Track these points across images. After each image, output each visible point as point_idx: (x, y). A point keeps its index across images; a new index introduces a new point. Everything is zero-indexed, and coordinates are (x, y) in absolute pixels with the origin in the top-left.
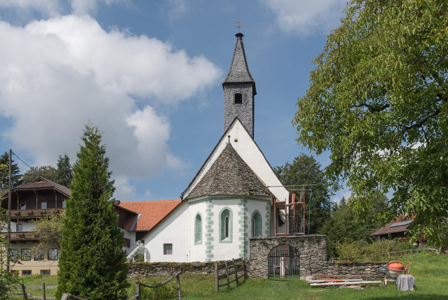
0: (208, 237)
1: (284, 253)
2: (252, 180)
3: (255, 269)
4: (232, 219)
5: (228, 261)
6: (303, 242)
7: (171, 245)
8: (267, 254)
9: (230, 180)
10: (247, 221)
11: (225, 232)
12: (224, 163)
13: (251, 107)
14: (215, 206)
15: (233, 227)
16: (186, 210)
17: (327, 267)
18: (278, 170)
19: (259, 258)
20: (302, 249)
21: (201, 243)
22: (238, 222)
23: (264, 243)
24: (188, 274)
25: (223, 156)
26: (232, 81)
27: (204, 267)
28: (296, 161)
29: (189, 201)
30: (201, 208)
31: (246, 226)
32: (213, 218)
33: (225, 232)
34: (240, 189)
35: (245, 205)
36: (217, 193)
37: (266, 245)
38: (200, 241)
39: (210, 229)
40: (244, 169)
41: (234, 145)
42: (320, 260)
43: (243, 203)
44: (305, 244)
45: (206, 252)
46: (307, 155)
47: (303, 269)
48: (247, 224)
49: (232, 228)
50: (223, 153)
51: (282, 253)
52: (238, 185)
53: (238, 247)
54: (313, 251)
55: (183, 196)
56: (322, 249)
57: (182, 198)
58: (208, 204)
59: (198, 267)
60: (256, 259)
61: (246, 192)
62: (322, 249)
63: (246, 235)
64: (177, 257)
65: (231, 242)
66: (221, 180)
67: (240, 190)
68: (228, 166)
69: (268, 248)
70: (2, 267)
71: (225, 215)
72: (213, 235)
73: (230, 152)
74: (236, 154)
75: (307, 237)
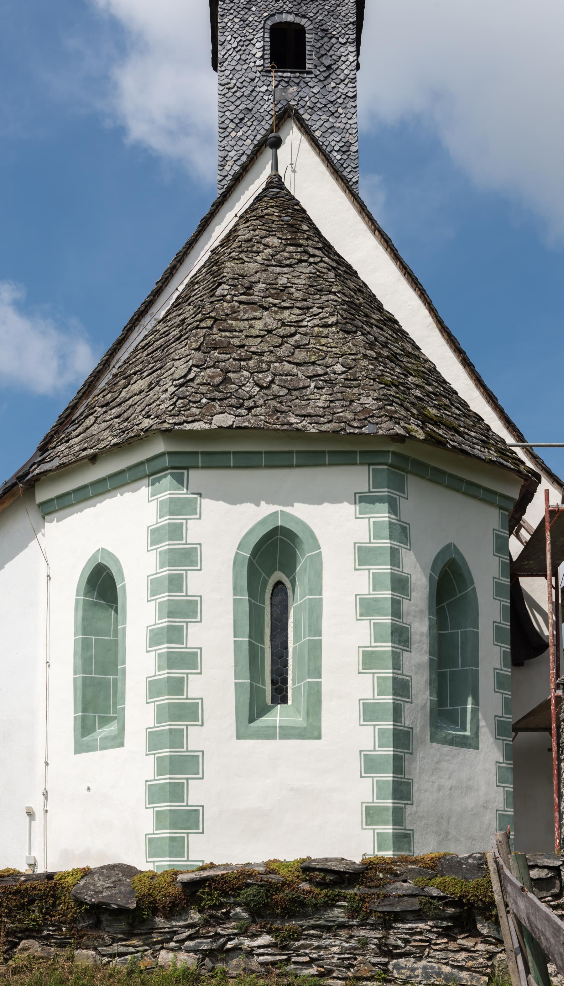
0: (165, 700)
4: (316, 587)
9: (300, 356)
10: (406, 605)
11: (272, 678)
14: (207, 505)
15: (326, 639)
16: (23, 546)
21: (118, 741)
22: (351, 608)
24: (39, 969)
27: (174, 910)
29: (44, 494)
30: (121, 524)
31: (400, 636)
32: (195, 583)
33: (272, 678)
34: (369, 402)
35: (394, 509)
36: (224, 420)
38: (112, 728)
39: (176, 647)
43: (384, 492)
45: (154, 794)
48: (407, 620)
49: (315, 649)
52: (351, 381)
58: (165, 496)
59: (122, 911)
65: (312, 731)
66: (243, 353)
67: (365, 410)
68: (282, 280)
71: (274, 561)
72: (196, 687)
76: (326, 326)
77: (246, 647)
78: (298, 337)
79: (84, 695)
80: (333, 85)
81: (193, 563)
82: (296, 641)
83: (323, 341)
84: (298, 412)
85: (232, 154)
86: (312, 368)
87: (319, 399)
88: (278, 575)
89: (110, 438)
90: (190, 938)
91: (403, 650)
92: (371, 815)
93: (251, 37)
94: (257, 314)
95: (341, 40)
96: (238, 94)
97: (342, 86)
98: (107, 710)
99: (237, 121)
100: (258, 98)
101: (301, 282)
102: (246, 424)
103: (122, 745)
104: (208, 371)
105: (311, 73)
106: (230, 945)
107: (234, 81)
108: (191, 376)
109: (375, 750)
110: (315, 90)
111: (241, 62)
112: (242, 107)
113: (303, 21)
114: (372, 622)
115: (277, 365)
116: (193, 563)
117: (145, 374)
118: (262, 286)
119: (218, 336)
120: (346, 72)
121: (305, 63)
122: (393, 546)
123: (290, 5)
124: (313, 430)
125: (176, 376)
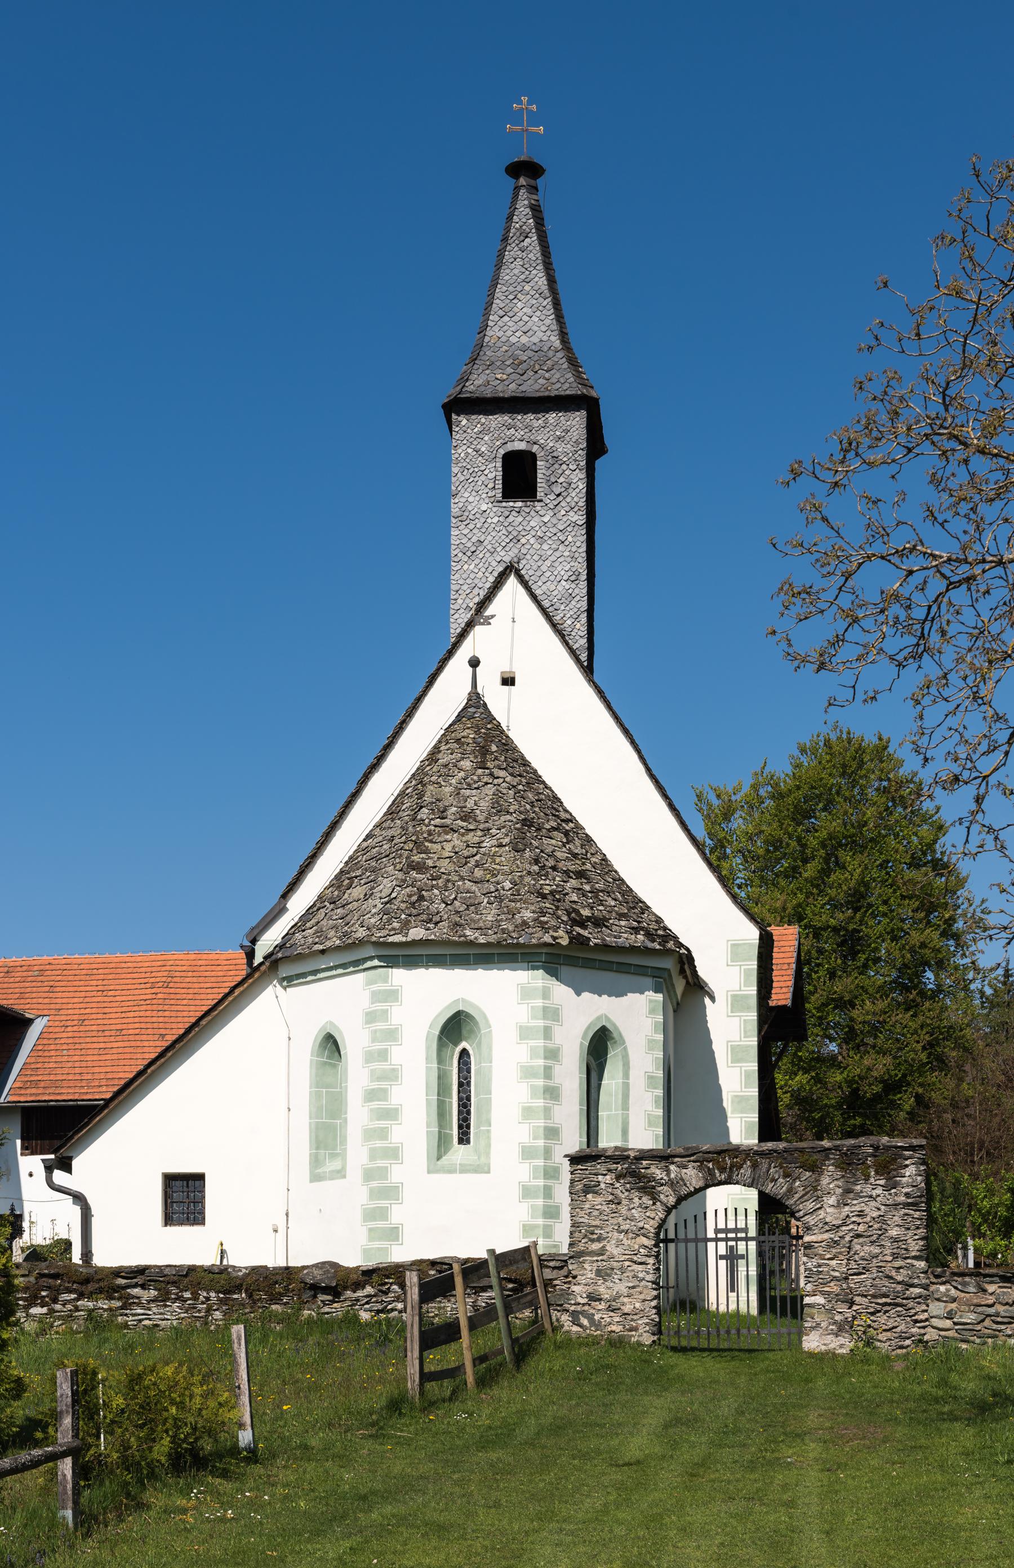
1: (731, 1225)
2: (581, 875)
5: (467, 1261)
6: (815, 1168)
7: (200, 1177)
8: (651, 1226)
9: (478, 873)
11: (459, 1117)
12: (448, 790)
13: (580, 518)
17: (926, 1287)
18: (715, 802)
19: (612, 1249)
21: (341, 1174)
23: (634, 1174)
25: (444, 759)
26: (488, 393)
27: (358, 1286)
28: (805, 760)
29: (284, 971)
30: (340, 999)
33: (459, 1117)
34: (527, 915)
36: (417, 933)
37: (647, 1187)
38: (335, 1165)
40: (541, 817)
41: (498, 701)
42: (895, 1256)
44: (825, 1181)
46: (857, 733)
47: (819, 1300)
50: (443, 739)
51: (721, 1225)
53: (516, 1192)
54: (861, 1214)
55: (254, 941)
56: (907, 1205)
57: (250, 955)
60: (602, 1252)
61: (556, 929)
62: (907, 1205)
63: (552, 1133)
64: (240, 1234)
67: (524, 923)
69: (655, 1199)
73: (479, 733)
74: (507, 746)
75: (837, 1148)
76: (501, 846)
77: (435, 1103)
78: (477, 858)
79: (317, 1137)
80: (563, 512)
81: (395, 1039)
82: (476, 1096)
83: (498, 860)
84: (472, 926)
85: (465, 587)
86: (486, 885)
88: (464, 1044)
89: (335, 939)
90: (367, 1303)
93: (483, 468)
94: (448, 837)
95: (571, 467)
96: (471, 526)
97: (571, 513)
98: (335, 1148)
99: (469, 554)
100: (490, 529)
101: (484, 804)
102: (433, 937)
103: (344, 1177)
104: (408, 890)
105: (541, 501)
106: (389, 1307)
107: (466, 514)
108: (394, 895)
110: (546, 519)
111: (474, 493)
112: (474, 539)
113: (535, 449)
115: (460, 883)
116: (395, 1039)
117: (362, 882)
118: (454, 809)
119: (416, 858)
120: (576, 499)
121: (536, 491)
123: (522, 433)
124: (482, 941)
125: (383, 895)
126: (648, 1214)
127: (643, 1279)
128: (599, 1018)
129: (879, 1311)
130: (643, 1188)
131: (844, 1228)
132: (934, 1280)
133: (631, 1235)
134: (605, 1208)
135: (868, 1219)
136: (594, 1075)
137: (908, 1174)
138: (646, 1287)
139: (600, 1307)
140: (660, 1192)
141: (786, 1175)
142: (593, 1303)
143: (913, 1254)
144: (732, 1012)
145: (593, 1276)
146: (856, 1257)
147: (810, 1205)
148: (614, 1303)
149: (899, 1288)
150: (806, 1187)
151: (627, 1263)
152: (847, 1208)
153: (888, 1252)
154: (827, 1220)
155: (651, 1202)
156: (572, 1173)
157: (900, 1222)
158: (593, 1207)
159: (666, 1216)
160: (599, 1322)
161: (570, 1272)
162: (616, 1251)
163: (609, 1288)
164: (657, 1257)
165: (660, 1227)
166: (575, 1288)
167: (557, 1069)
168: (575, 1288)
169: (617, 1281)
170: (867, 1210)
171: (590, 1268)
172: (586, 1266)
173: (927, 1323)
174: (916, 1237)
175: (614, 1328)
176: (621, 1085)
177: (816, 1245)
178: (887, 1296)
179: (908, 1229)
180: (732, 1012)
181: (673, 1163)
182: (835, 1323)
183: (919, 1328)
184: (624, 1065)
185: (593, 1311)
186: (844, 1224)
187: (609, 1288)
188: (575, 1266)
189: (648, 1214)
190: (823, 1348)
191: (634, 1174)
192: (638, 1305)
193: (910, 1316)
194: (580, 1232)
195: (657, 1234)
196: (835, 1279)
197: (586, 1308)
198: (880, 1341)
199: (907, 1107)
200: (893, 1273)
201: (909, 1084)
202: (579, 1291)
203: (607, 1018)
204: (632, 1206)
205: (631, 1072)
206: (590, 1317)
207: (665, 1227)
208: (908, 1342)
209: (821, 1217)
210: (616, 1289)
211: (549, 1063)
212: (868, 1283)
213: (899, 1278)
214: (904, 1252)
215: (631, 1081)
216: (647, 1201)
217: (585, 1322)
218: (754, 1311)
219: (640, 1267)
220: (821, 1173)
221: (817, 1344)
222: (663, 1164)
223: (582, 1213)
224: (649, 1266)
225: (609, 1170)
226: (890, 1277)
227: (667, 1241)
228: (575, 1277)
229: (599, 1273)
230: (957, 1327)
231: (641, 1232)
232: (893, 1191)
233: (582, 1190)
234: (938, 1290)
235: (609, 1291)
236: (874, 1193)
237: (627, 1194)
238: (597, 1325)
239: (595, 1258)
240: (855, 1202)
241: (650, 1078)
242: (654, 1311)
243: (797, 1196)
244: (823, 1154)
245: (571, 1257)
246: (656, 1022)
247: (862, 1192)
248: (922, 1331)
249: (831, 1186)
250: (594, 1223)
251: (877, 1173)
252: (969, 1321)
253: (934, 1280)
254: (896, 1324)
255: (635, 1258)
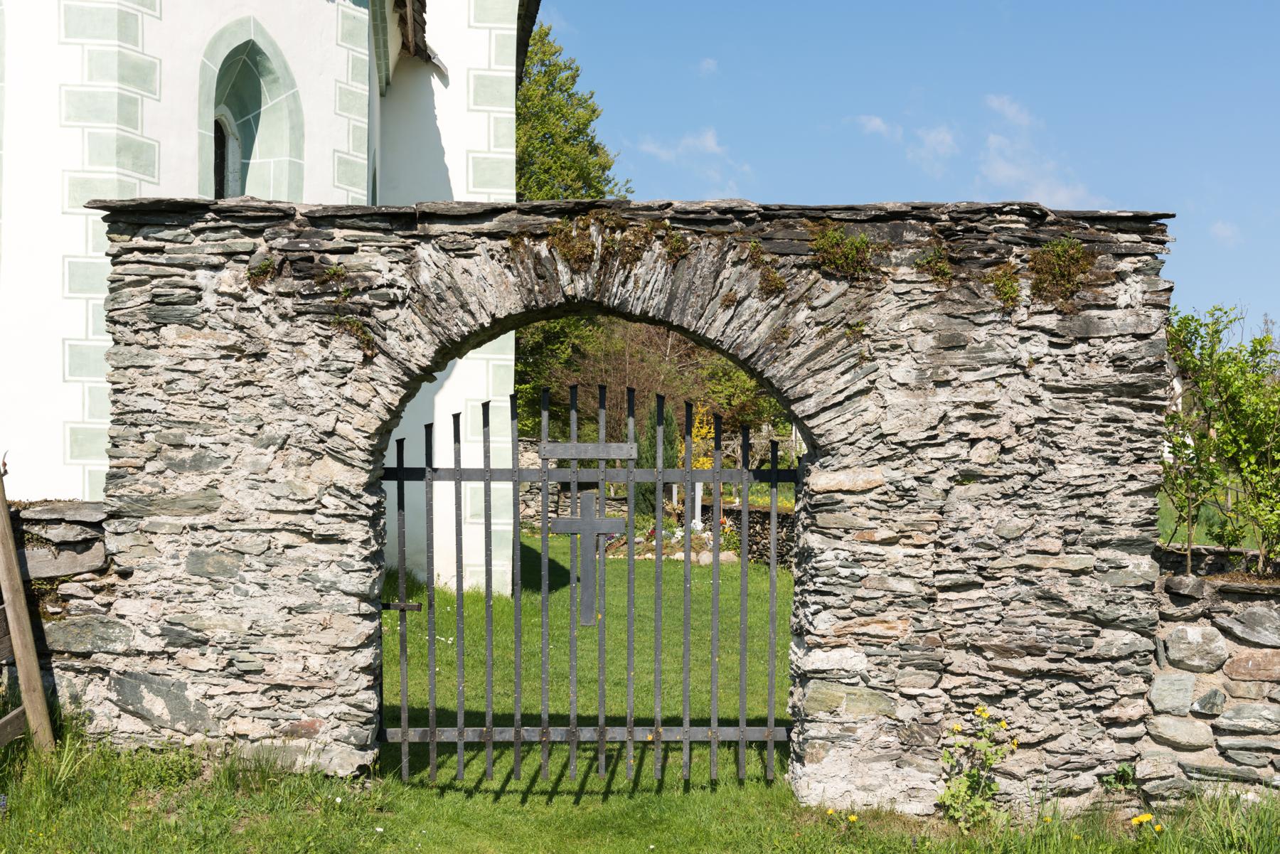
3: (181, 637)
8: (356, 429)
19: (237, 494)
20: (834, 383)
37: (346, 309)
42: (1069, 539)
44: (885, 309)
47: (853, 659)
54: (983, 412)
60: (207, 502)
69: (370, 349)
70: (1150, 704)
87: (365, 407)
91: (141, 180)
92: (78, 441)
109: (87, 339)
114: (87, 130)
122: (124, 9)
126: (348, 391)
127: (333, 586)
128: (241, 23)
129: (1010, 693)
130: (336, 310)
131: (930, 453)
132: (1171, 609)
133: (295, 454)
134: (215, 367)
135: (1002, 428)
136: (233, 147)
137: (1123, 300)
138: (341, 610)
139: (203, 664)
140: (385, 326)
141: (770, 289)
142: (182, 654)
143: (1123, 533)
144: (476, 104)
145: (180, 572)
146: (960, 539)
147: (834, 383)
148: (244, 655)
149: (1076, 628)
150: (825, 326)
151: (284, 538)
152: (944, 394)
153: (1051, 525)
154: (886, 428)
155: (358, 356)
156: (116, 259)
157: (1093, 441)
158: (178, 367)
159: (404, 401)
160: (202, 707)
161: (109, 558)
162: (249, 502)
163: (228, 610)
164: (374, 521)
165: (384, 431)
166: (122, 606)
167: (149, 109)
168: (122, 606)
169: (254, 589)
170: (1002, 400)
171: (171, 549)
172: (159, 542)
173: (1140, 728)
174: (1134, 486)
175: (243, 726)
176: (286, 166)
177: (850, 500)
178: (1041, 652)
179: (1114, 461)
180: (476, 104)
181: (427, 238)
182: (897, 725)
183: (1120, 740)
184: (292, 128)
185: (183, 676)
186: (931, 441)
187: (228, 610)
188: (126, 542)
189: (348, 391)
190: (860, 798)
191: (304, 266)
192: (315, 662)
193: (1096, 709)
194: (141, 439)
195: (377, 453)
196: (900, 599)
197: (161, 665)
198: (1012, 776)
199: (564, 356)
200: (1062, 587)
201: (566, 336)
202: (139, 616)
203: (259, 28)
204: (299, 366)
205: (307, 147)
206: (173, 694)
207: (396, 434)
208: (1086, 779)
209: (868, 417)
210: (250, 615)
211: (132, 91)
212: (991, 613)
213: (1080, 603)
214: (1094, 527)
215: (307, 162)
216: (345, 349)
217: (156, 705)
218: (503, 582)
219: (325, 551)
220: (875, 288)
221: (843, 786)
222: (395, 240)
223: (145, 384)
224: (350, 549)
225: (230, 255)
226: (1050, 598)
227: (401, 474)
228: (125, 574)
229: (197, 562)
230: (1225, 741)
231: (325, 445)
232: (1079, 348)
233: (147, 314)
234: (1181, 638)
235: (229, 619)
236: (1024, 353)
237: (283, 327)
238: (195, 718)
239: (187, 520)
240: (968, 377)
241: (342, 162)
242: (365, 680)
243: (799, 353)
244: (886, 227)
245: (113, 516)
246: (355, 59)
247: (989, 347)
248: (1128, 750)
249: (903, 326)
250: (182, 414)
251: (1037, 291)
252: (1259, 725)
253: (1171, 609)
254: (1054, 729)
255: (308, 523)
